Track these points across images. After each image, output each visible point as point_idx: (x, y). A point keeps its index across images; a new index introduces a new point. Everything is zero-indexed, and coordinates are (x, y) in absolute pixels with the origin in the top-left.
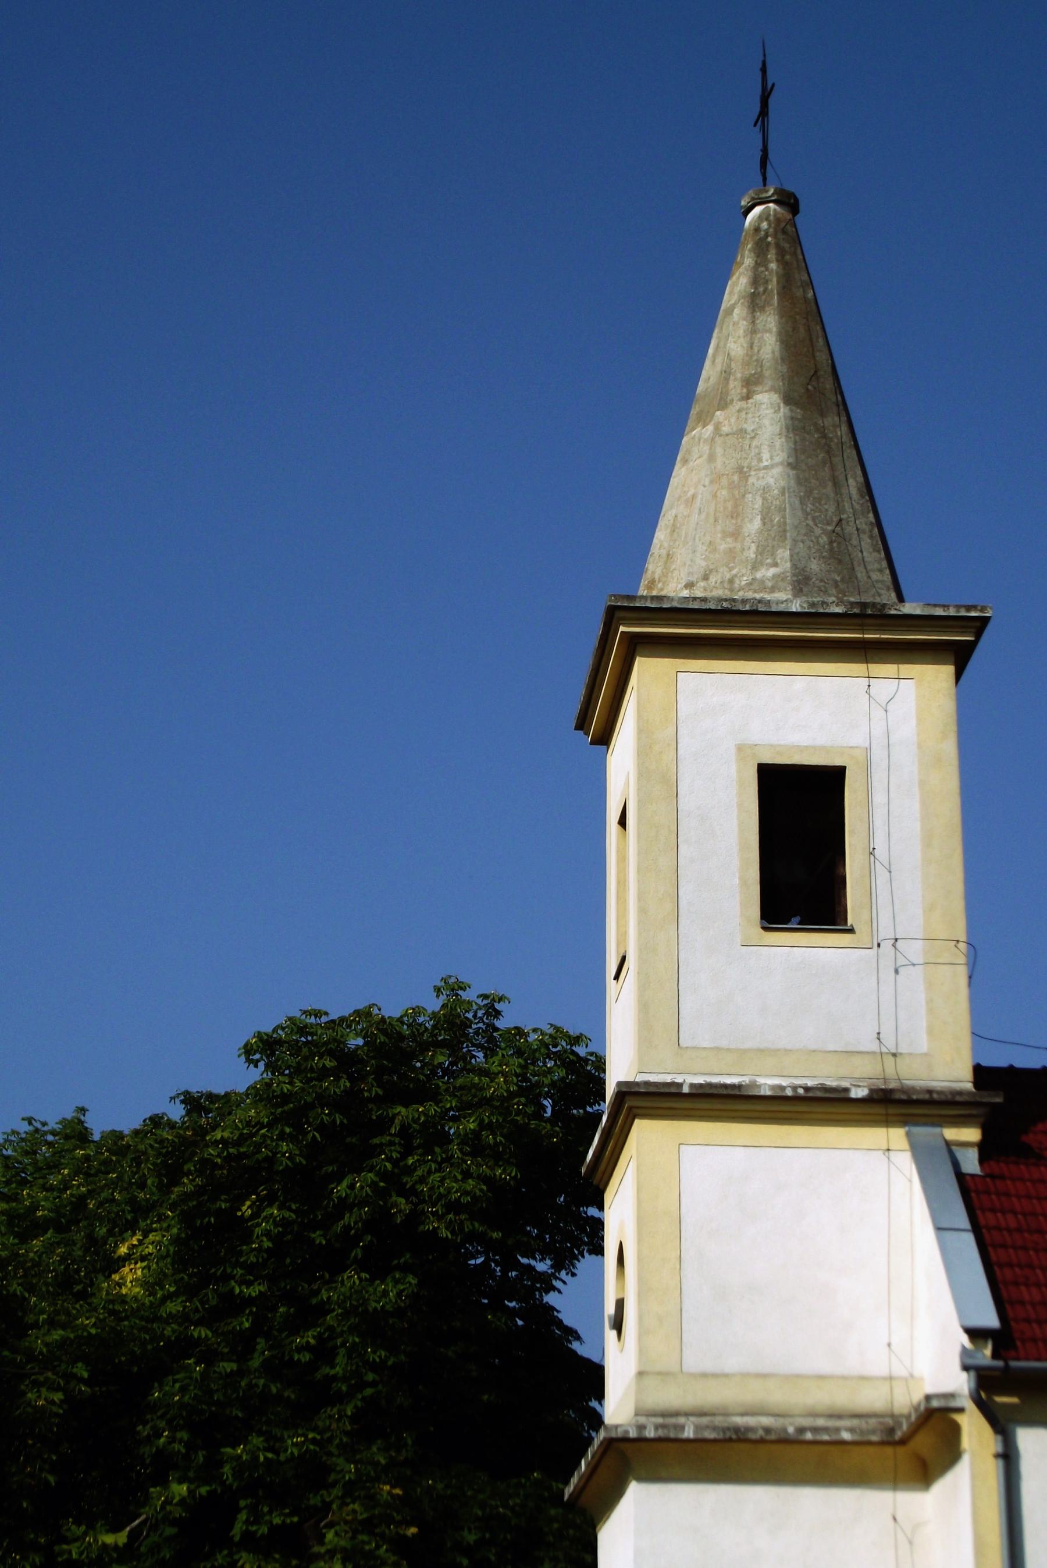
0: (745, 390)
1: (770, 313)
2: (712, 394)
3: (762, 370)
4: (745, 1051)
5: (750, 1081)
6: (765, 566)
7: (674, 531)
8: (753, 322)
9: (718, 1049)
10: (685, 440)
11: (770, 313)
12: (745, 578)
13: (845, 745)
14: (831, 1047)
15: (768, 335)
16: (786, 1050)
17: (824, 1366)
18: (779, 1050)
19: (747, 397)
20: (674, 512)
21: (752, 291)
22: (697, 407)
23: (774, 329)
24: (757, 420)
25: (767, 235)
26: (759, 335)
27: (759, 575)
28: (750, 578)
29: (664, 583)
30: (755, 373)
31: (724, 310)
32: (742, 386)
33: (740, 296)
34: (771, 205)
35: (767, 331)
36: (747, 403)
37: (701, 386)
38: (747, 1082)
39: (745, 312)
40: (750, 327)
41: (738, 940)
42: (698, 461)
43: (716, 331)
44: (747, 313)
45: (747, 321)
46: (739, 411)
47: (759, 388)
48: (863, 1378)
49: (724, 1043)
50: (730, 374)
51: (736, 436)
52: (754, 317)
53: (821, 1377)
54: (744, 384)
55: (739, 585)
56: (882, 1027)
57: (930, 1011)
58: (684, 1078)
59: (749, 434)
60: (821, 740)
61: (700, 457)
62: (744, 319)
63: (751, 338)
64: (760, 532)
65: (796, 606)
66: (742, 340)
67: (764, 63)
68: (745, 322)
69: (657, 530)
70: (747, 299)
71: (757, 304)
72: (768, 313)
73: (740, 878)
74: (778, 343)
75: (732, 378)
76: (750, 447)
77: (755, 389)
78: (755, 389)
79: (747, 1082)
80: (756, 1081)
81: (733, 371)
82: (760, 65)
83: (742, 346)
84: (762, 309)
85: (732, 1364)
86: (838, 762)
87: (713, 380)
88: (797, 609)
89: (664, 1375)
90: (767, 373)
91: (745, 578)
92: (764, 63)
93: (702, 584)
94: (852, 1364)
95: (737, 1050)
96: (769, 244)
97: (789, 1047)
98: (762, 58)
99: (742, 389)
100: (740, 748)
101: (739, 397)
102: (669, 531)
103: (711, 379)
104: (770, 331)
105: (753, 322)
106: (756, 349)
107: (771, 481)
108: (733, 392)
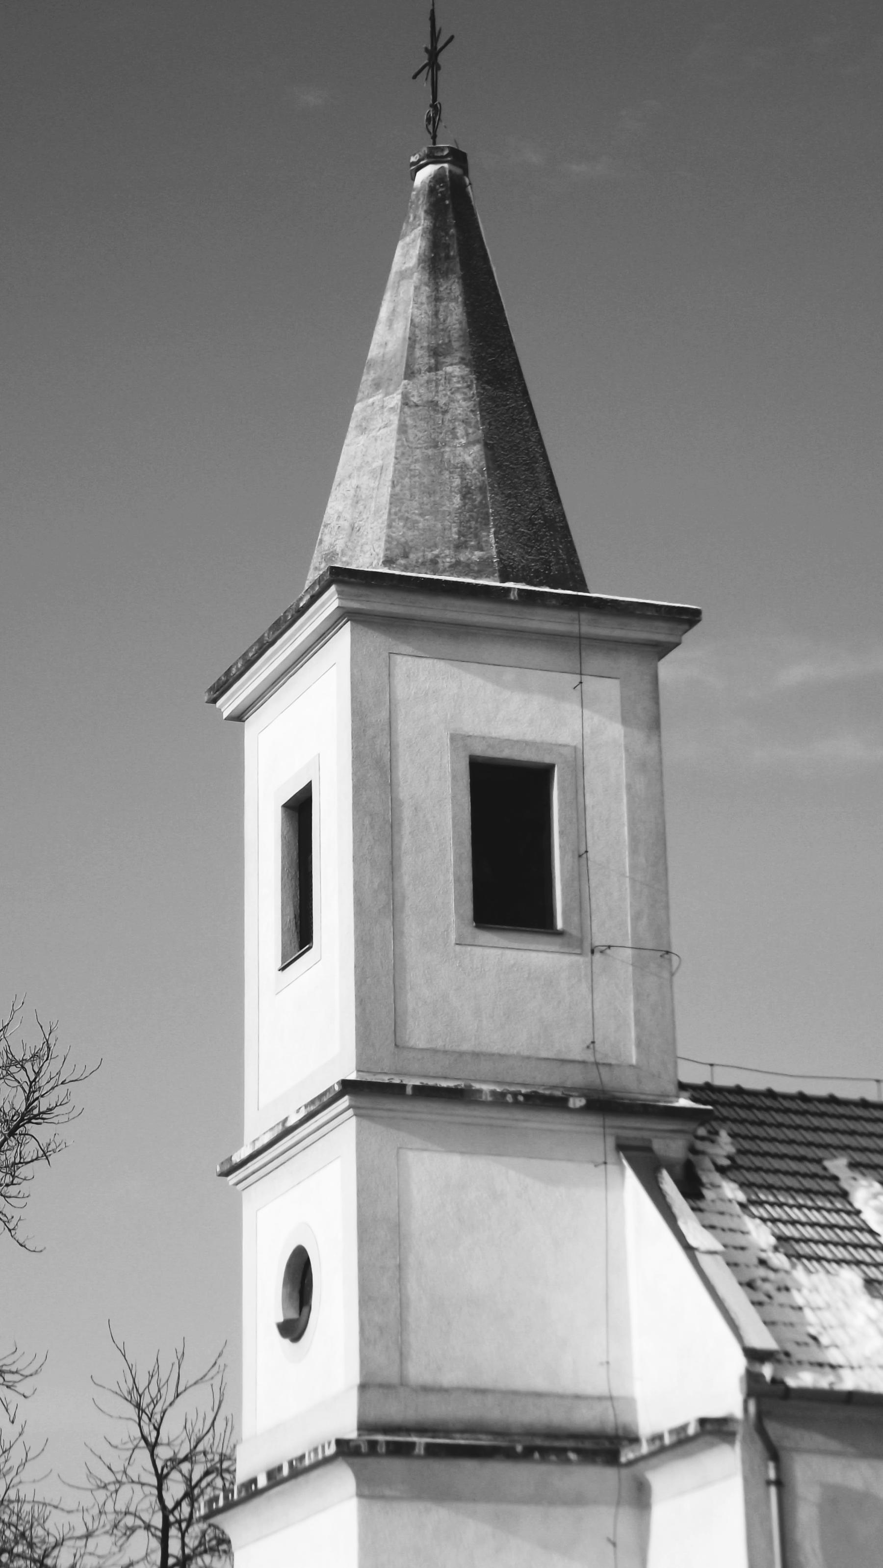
0: (433, 361)
1: (454, 282)
2: (393, 361)
3: (450, 341)
4: (461, 1054)
5: (465, 1086)
6: (469, 549)
7: (357, 502)
8: (437, 290)
9: (435, 1051)
10: (358, 407)
11: (454, 282)
12: (448, 560)
13: (554, 742)
14: (544, 1054)
15: (453, 304)
16: (500, 1055)
17: (540, 1384)
18: (493, 1055)
19: (435, 368)
20: (354, 482)
21: (433, 255)
22: (372, 372)
23: (460, 299)
24: (449, 393)
25: (443, 199)
26: (445, 304)
27: (462, 558)
28: (453, 560)
29: (351, 557)
30: (442, 344)
31: (396, 273)
32: (429, 356)
33: (419, 260)
34: (446, 165)
35: (452, 300)
36: (436, 375)
37: (374, 351)
38: (463, 1086)
39: (427, 276)
40: (434, 294)
41: (453, 937)
42: (383, 431)
43: (388, 296)
44: (429, 279)
45: (429, 286)
46: (428, 382)
47: (448, 360)
48: (577, 1397)
49: (439, 1044)
50: (415, 341)
51: (426, 408)
52: (437, 283)
53: (539, 1395)
54: (432, 353)
55: (443, 566)
56: (596, 1035)
57: (638, 1022)
58: (401, 1079)
59: (442, 408)
60: (531, 734)
61: (386, 426)
62: (426, 285)
63: (435, 306)
64: (460, 511)
65: (514, 594)
66: (425, 306)
67: (433, 12)
68: (427, 288)
69: (330, 500)
70: (427, 264)
71: (440, 269)
72: (452, 281)
73: (455, 874)
74: (465, 314)
75: (417, 346)
76: (443, 421)
77: (444, 360)
78: (444, 360)
79: (463, 1086)
80: (471, 1086)
81: (418, 339)
82: (429, 16)
83: (426, 313)
84: (446, 275)
85: (449, 1378)
86: (547, 759)
87: (391, 347)
88: (515, 598)
89: (386, 1387)
90: (456, 345)
91: (448, 560)
92: (433, 12)
93: (402, 561)
94: (567, 1383)
95: (454, 1052)
96: (447, 206)
97: (503, 1052)
98: (431, 8)
99: (429, 360)
100: (453, 738)
101: (427, 367)
102: (349, 501)
103: (390, 345)
104: (455, 299)
105: (437, 290)
106: (441, 318)
107: (468, 459)
108: (420, 361)
